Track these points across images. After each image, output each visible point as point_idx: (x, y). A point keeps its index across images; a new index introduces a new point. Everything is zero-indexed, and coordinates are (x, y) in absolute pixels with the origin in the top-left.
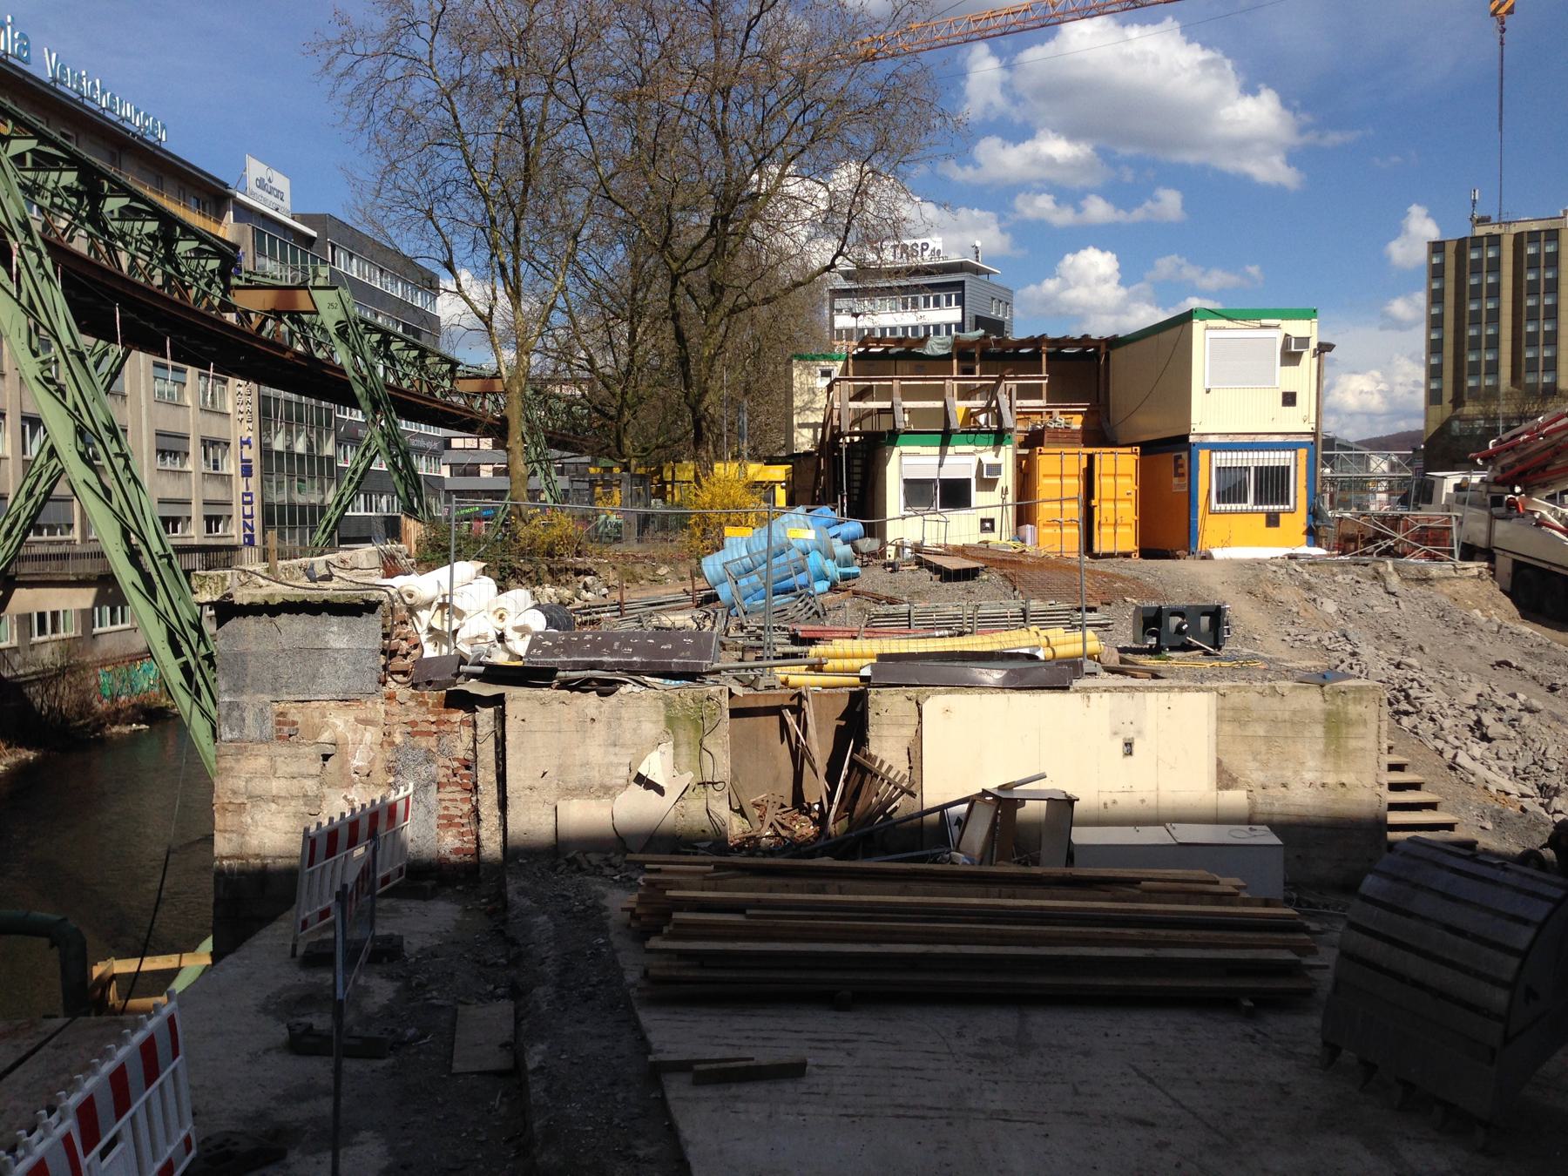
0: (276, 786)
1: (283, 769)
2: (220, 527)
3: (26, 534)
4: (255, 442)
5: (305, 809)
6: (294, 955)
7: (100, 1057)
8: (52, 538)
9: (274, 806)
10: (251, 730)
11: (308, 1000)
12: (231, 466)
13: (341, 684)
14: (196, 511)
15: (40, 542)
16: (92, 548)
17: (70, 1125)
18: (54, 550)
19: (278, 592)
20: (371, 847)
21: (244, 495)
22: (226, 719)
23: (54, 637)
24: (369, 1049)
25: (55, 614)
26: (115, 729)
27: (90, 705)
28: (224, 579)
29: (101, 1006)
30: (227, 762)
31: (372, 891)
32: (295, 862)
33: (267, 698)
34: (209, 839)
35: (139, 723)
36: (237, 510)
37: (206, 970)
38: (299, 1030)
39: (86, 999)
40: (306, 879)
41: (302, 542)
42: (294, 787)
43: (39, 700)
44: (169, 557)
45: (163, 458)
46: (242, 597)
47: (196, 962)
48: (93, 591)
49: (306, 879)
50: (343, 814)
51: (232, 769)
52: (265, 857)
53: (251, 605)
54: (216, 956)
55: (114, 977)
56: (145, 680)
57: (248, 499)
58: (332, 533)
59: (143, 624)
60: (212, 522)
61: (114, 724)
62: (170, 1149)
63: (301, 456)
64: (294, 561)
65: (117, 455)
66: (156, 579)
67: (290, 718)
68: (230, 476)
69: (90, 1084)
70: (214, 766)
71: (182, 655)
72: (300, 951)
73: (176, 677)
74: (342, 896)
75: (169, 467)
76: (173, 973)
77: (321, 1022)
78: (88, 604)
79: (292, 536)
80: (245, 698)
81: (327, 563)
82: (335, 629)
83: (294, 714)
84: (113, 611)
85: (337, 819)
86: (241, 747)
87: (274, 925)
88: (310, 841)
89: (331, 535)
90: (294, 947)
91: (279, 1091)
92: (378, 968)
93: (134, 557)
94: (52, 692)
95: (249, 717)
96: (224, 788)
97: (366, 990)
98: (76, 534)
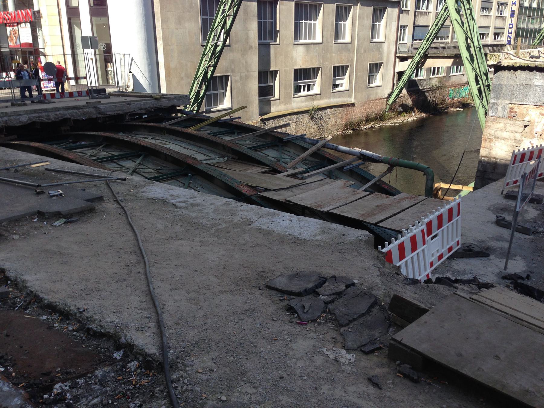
0: (506, 134)
1: (509, 128)
2: (499, 37)
3: (433, 40)
4: (517, 3)
5: (515, 144)
6: (502, 194)
7: (430, 213)
8: (441, 41)
9: (503, 141)
10: (500, 113)
11: (505, 209)
12: (507, 13)
13: (536, 99)
14: (491, 31)
15: (438, 43)
16: (455, 45)
17: (424, 227)
18: (442, 45)
19: (518, 62)
20: (537, 162)
21: (510, 24)
22: (491, 108)
23: (437, 76)
24: (525, 231)
25: (439, 68)
26: (452, 109)
27: (445, 100)
28: (499, 56)
29: (436, 196)
30: (489, 124)
31: (535, 177)
32: (507, 162)
33: (507, 102)
34: (478, 151)
35: (460, 108)
36: (506, 31)
37: (470, 192)
38: (500, 218)
39: (431, 193)
40: (511, 168)
41: (529, 44)
42: (512, 135)
43: (429, 97)
44: (480, 48)
45: (483, 11)
46: (504, 63)
47: (467, 189)
48: (452, 60)
49: (511, 168)
50: (529, 148)
51: (490, 126)
52: (497, 159)
53: (507, 66)
54: (475, 188)
55: (441, 188)
56: (464, 93)
57: (511, 26)
58: (542, 40)
59: (468, 72)
60: (496, 35)
61: (452, 107)
62: (452, 243)
63: (534, 9)
64: (526, 50)
65: (468, 9)
66: (474, 56)
67: (515, 110)
68: (506, 17)
69: (431, 217)
70: (484, 125)
71: (479, 84)
72: (505, 193)
73: (476, 92)
74: (524, 177)
75: (484, 14)
76: (458, 192)
77: (509, 218)
78: (450, 65)
79: (525, 41)
80: (499, 101)
81: (539, 51)
82: (538, 77)
83: (516, 109)
84: (457, 68)
85: (526, 149)
86: (495, 119)
87: (496, 182)
88: (515, 156)
89: (541, 41)
90: (503, 191)
91: (490, 236)
92: (532, 204)
93: (468, 48)
94: (434, 95)
95: (500, 108)
96: (486, 133)
97: (526, 211)
98: (449, 40)
